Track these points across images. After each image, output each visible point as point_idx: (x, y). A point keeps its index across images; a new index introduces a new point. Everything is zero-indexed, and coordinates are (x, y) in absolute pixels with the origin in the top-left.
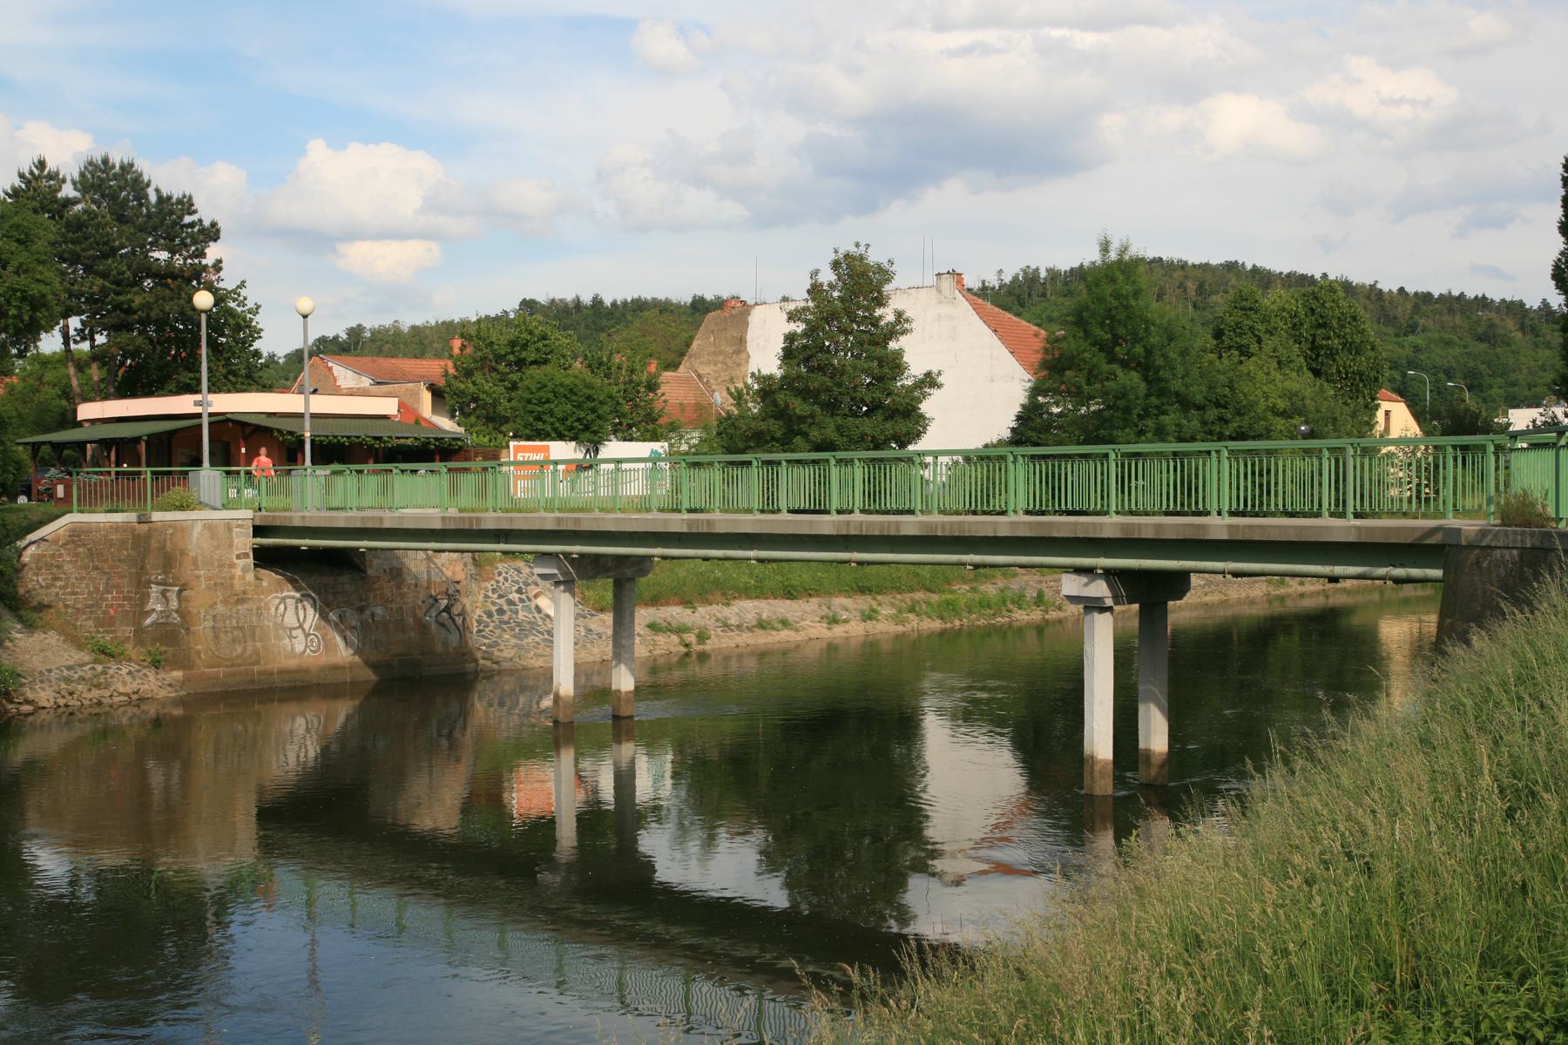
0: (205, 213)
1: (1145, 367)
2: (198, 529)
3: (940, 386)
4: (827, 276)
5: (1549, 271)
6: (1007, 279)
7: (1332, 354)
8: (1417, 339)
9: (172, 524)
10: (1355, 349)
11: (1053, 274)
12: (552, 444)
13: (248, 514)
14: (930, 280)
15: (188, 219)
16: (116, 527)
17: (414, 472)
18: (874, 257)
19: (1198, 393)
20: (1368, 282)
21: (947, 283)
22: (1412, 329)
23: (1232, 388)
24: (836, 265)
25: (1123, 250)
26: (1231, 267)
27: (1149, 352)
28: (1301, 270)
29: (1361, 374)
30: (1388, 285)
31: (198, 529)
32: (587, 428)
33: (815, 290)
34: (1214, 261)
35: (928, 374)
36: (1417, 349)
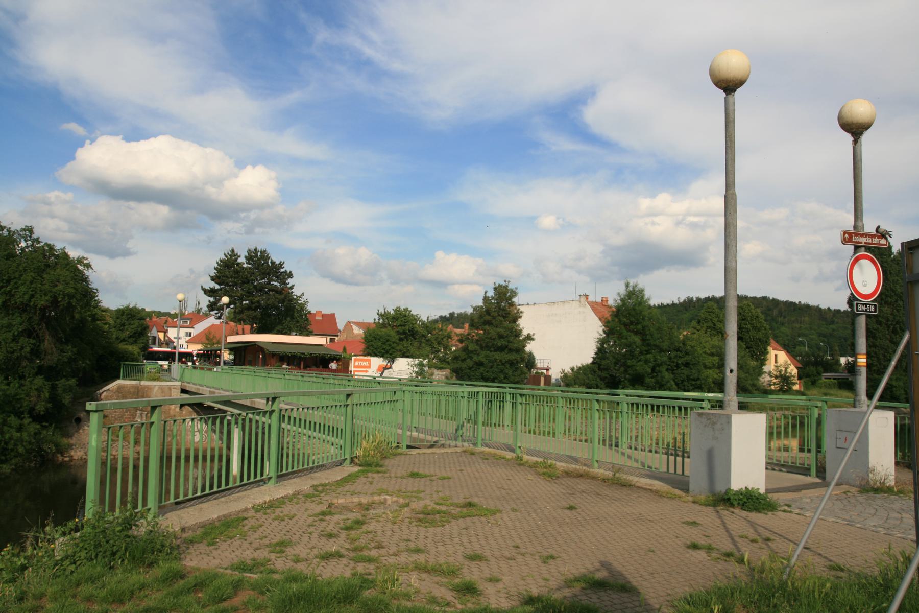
0: (287, 268)
1: (641, 333)
2: (156, 388)
3: (533, 339)
4: (491, 293)
5: (846, 301)
6: (682, 301)
7: (748, 331)
8: (834, 327)
9: (147, 387)
10: (758, 330)
11: (698, 299)
12: (372, 359)
13: (179, 383)
14: (578, 298)
15: (282, 270)
16: (133, 386)
17: (210, 370)
18: (511, 286)
19: (665, 345)
20: (816, 305)
21: (583, 299)
22: (833, 323)
23: (684, 344)
24: (495, 289)
25: (634, 287)
26: (764, 298)
27: (644, 328)
28: (791, 300)
29: (760, 340)
30: (823, 306)
31: (156, 388)
32: (387, 352)
33: (486, 299)
34: (758, 296)
35: (529, 335)
36: (834, 330)
